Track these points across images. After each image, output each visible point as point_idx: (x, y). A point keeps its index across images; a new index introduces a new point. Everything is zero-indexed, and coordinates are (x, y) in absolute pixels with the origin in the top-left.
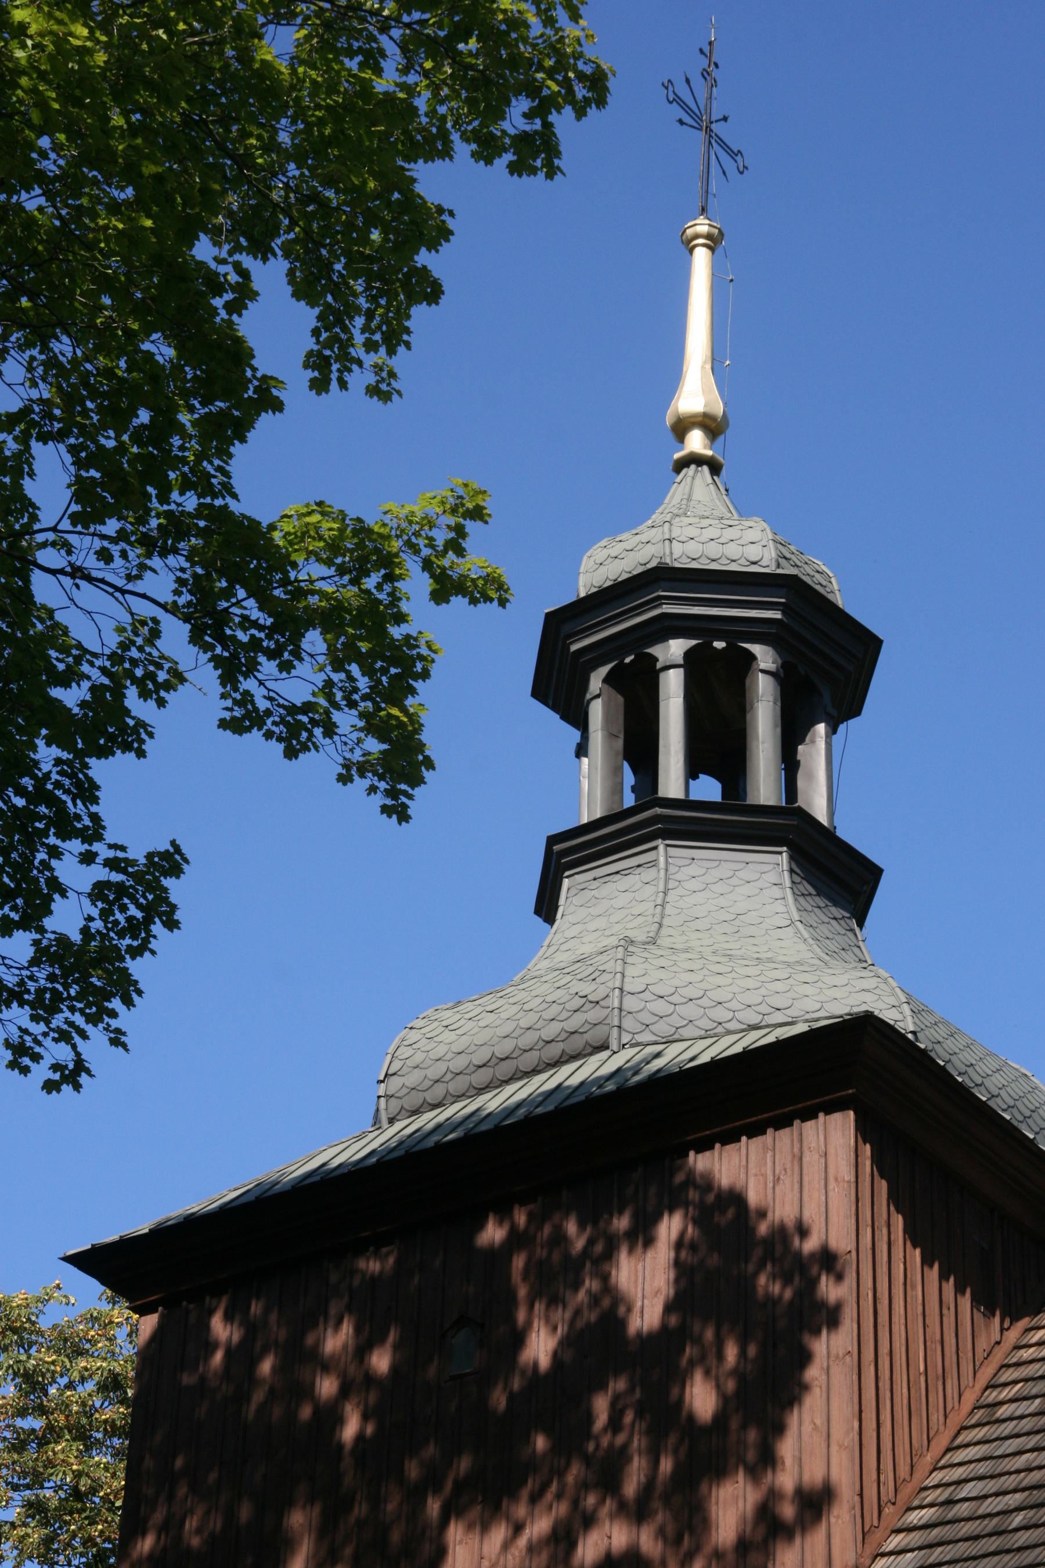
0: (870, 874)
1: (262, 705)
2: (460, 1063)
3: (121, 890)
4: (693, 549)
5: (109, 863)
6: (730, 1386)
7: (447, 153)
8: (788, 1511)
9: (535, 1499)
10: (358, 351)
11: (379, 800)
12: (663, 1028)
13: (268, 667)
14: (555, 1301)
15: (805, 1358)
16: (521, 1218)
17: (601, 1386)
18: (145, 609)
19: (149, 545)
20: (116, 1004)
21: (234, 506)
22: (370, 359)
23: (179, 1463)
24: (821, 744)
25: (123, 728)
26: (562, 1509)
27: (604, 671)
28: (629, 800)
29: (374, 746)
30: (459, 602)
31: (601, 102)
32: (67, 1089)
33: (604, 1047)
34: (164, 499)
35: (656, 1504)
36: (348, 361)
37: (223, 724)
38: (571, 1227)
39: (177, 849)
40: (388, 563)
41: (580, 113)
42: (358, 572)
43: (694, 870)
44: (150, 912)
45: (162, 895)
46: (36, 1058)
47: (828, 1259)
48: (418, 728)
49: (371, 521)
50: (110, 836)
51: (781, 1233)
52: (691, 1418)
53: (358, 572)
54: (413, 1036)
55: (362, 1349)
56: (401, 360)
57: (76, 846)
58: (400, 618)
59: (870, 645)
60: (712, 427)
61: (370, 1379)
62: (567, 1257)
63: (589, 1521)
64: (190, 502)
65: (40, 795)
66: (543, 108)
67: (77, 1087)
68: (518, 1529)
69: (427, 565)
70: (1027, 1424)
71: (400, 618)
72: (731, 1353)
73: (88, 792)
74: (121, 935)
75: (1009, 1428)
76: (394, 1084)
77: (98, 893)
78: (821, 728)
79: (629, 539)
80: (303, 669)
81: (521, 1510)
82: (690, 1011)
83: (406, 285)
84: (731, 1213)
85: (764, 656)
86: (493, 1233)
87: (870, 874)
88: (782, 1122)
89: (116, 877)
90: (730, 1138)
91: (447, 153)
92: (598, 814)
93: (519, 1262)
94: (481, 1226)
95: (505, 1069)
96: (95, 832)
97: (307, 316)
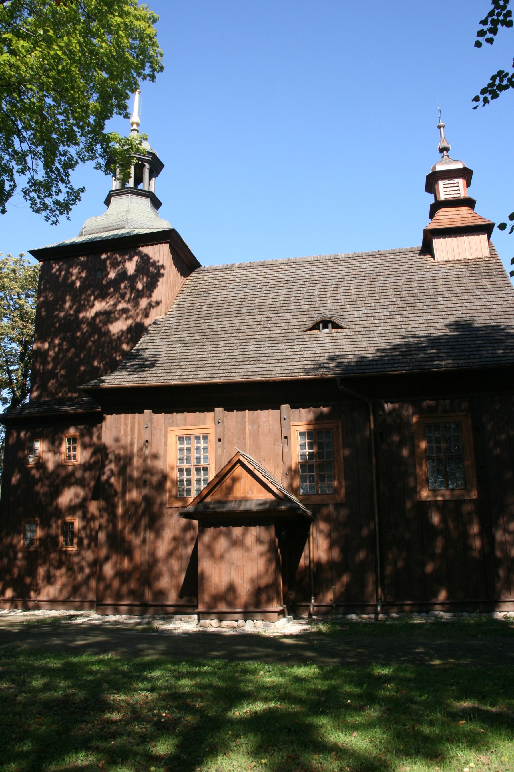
0: (160, 204)
2: (98, 227)
5: (69, 188)
6: (145, 284)
8: (154, 304)
9: (111, 297)
12: (134, 226)
14: (115, 268)
15: (158, 281)
16: (109, 254)
17: (123, 282)
23: (48, 286)
24: (154, 181)
26: (115, 300)
31: (162, 71)
32: (54, 225)
33: (124, 228)
35: (131, 301)
37: (94, 168)
39: (84, 188)
43: (135, 200)
44: (76, 197)
46: (49, 219)
47: (163, 266)
50: (71, 184)
52: (138, 289)
54: (89, 222)
55: (79, 273)
59: (163, 166)
60: (138, 125)
61: (81, 277)
62: (117, 262)
63: (120, 302)
67: (56, 225)
68: (107, 303)
70: (189, 294)
72: (145, 279)
73: (67, 175)
74: (71, 201)
75: (186, 294)
81: (108, 300)
82: (138, 224)
84: (146, 258)
85: (147, 166)
86: (103, 256)
87: (160, 204)
89: (70, 191)
90: (147, 245)
92: (118, 188)
93: (108, 262)
94: (102, 255)
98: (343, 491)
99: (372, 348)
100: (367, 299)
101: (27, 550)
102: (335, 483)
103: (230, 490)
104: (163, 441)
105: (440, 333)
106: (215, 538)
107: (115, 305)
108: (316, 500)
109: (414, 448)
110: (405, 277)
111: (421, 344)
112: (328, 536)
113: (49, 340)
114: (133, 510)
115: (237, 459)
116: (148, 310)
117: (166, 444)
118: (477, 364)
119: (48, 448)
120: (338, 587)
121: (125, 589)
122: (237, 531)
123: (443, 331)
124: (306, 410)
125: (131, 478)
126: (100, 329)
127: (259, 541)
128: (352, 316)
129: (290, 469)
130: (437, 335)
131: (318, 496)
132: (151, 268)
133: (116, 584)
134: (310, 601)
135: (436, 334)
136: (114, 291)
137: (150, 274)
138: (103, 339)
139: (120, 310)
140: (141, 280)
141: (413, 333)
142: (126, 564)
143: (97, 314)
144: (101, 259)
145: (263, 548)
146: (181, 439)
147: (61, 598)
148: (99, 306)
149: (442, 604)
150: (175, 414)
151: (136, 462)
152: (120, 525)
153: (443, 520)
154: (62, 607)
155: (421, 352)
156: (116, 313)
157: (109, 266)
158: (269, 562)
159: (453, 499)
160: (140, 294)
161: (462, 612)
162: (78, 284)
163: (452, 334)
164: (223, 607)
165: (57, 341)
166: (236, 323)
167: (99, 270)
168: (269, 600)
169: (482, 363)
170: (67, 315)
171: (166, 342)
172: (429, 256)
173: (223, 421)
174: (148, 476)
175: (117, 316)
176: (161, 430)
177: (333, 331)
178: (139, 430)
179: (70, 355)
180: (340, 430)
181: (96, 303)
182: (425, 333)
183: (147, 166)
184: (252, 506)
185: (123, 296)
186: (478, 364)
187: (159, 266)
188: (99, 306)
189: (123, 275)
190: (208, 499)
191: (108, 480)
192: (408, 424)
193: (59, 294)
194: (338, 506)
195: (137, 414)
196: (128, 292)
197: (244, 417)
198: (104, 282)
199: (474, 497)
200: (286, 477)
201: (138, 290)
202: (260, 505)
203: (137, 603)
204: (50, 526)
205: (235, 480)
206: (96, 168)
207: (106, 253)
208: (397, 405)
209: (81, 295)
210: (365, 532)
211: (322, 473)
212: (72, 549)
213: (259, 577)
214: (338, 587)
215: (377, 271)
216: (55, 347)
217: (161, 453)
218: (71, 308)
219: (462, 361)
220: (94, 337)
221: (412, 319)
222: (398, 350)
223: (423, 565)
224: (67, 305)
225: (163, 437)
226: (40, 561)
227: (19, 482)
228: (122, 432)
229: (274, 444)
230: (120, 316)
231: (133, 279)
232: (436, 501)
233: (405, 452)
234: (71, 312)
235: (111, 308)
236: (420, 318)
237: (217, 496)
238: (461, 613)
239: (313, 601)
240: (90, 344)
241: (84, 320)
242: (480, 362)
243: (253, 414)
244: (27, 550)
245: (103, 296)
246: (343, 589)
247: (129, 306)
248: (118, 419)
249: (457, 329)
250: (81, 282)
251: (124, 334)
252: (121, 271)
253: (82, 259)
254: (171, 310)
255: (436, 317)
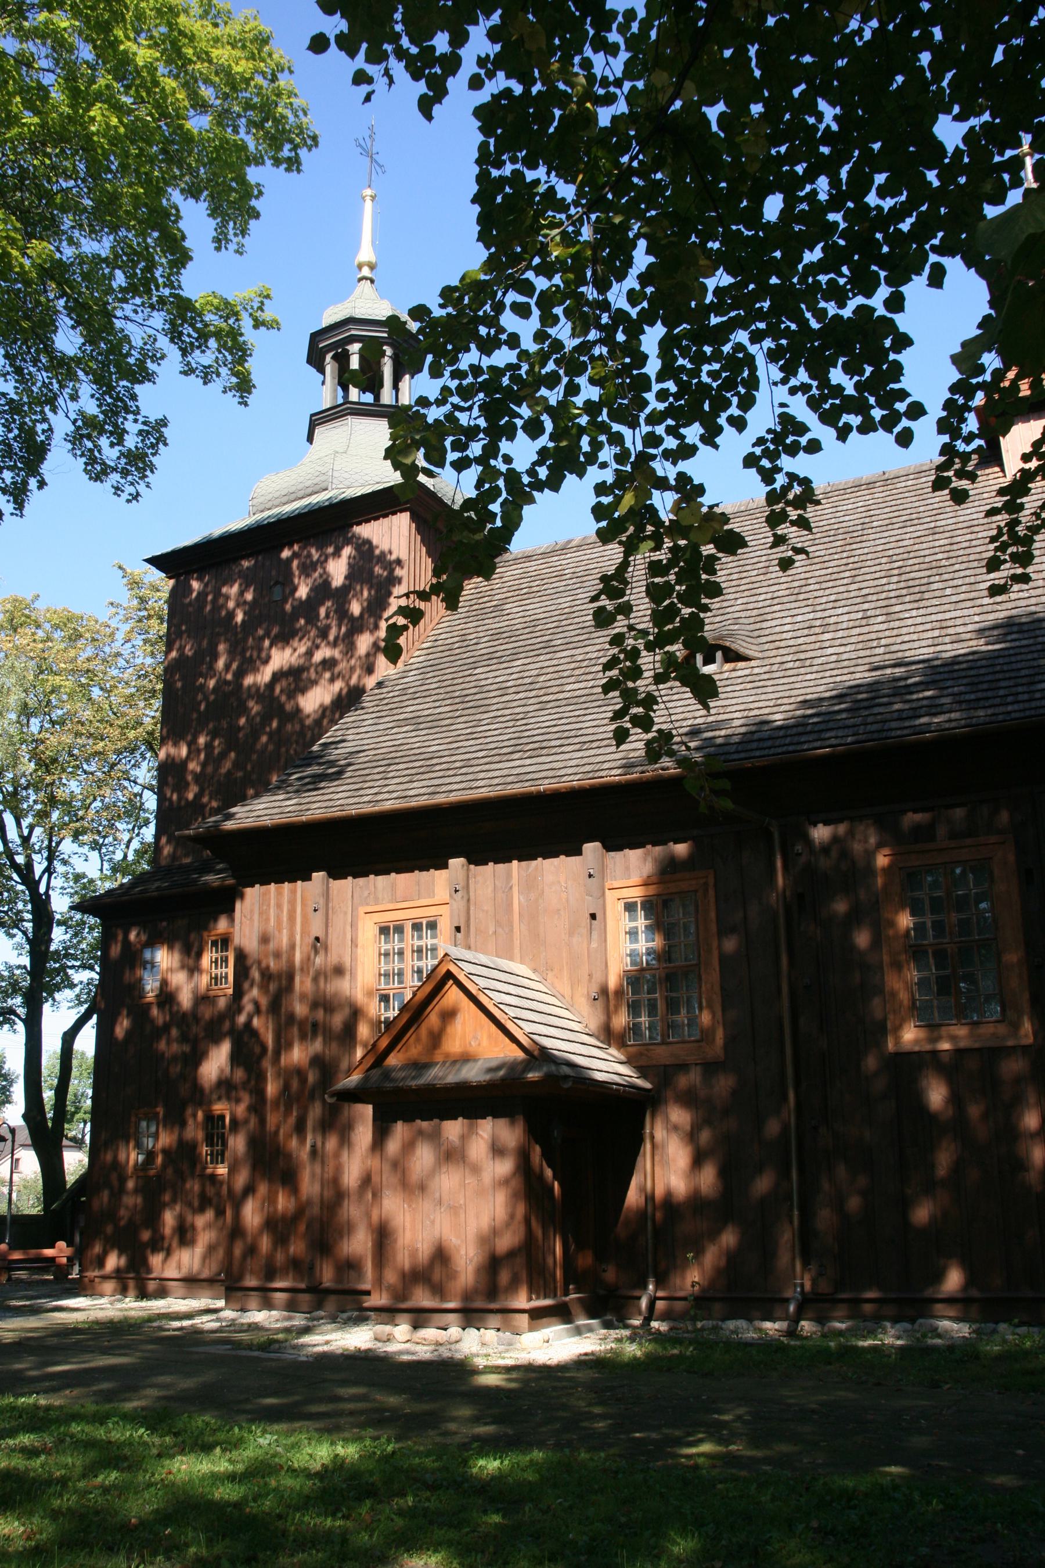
1: (194, 366)
2: (277, 495)
3: (148, 433)
4: (363, 311)
7: (263, 163)
9: (300, 640)
10: (231, 236)
11: (237, 399)
12: (347, 483)
13: (197, 352)
14: (308, 576)
17: (323, 604)
18: (151, 332)
19: (152, 307)
20: (148, 473)
21: (181, 293)
22: (235, 240)
25: (148, 374)
26: (309, 644)
27: (331, 354)
28: (340, 401)
29: (234, 380)
30: (263, 329)
31: (316, 145)
34: (157, 290)
36: (228, 241)
38: (313, 551)
40: (236, 314)
41: (310, 150)
42: (226, 319)
44: (158, 440)
45: (162, 435)
47: (399, 562)
48: (249, 374)
49: (230, 300)
50: (143, 413)
51: (383, 553)
53: (226, 319)
55: (241, 593)
56: (246, 241)
57: (131, 417)
58: (241, 335)
60: (372, 267)
61: (245, 602)
63: (318, 647)
64: (167, 292)
65: (118, 399)
66: (295, 148)
68: (295, 650)
69: (251, 315)
71: (241, 335)
72: (366, 594)
73: (134, 397)
76: (255, 501)
77: (140, 433)
78: (407, 377)
79: (340, 307)
80: (208, 353)
83: (248, 212)
85: (388, 351)
86: (286, 554)
88: (385, 516)
90: (368, 521)
91: (263, 163)
93: (295, 563)
94: (282, 550)
95: (292, 497)
96: (137, 412)
97: (212, 223)
98: (720, 1034)
99: (792, 700)
100: (824, 586)
101: (141, 1174)
102: (706, 1018)
103: (436, 1039)
104: (349, 937)
105: (961, 649)
106: (409, 1147)
107: (309, 653)
108: (662, 1055)
109: (880, 927)
110: (926, 526)
111: (906, 679)
112: (691, 1137)
113: (189, 738)
114: (295, 1084)
115: (444, 971)
116: (371, 659)
117: (354, 943)
118: (1013, 715)
119: (182, 961)
120: (711, 1256)
121: (280, 1257)
122: (453, 1129)
123: (971, 643)
124: (639, 852)
125: (291, 1017)
126: (282, 706)
127: (497, 1150)
128: (778, 629)
129: (604, 991)
130: (953, 653)
131: (664, 1047)
132: (377, 569)
133: (265, 1243)
134: (645, 1287)
135: (950, 650)
136: (307, 623)
137: (375, 581)
138: (289, 727)
139: (317, 665)
140: (358, 595)
141: (900, 655)
142: (283, 1203)
143: (277, 676)
144: (280, 559)
145: (505, 1167)
146: (384, 930)
147: (206, 1274)
148: (281, 658)
149: (950, 1301)
150: (372, 876)
151: (302, 984)
152: (272, 1119)
153: (955, 1099)
154: (208, 1293)
155: (897, 699)
156: (312, 670)
157: (297, 573)
158: (515, 1196)
159: (977, 1045)
160: (356, 626)
161: (997, 1323)
162: (239, 617)
163: (990, 647)
164: (423, 1299)
165: (202, 740)
166: (533, 670)
167: (277, 583)
168: (513, 1287)
169: (1028, 713)
170: (222, 683)
171: (386, 723)
172: (997, 469)
173: (467, 887)
174: (320, 1014)
175: (313, 676)
176: (346, 913)
177: (728, 666)
178: (304, 916)
179: (227, 765)
180: (711, 893)
181: (274, 652)
182: (926, 653)
183: (388, 351)
184: (472, 1073)
185: (324, 634)
186: (1017, 715)
187: (390, 563)
188: (281, 658)
189: (323, 590)
190: (393, 1060)
191: (248, 1024)
192: (870, 869)
193: (205, 643)
194: (710, 1068)
195: (299, 883)
196: (334, 623)
197: (509, 876)
198: (288, 607)
199: (1030, 1040)
200: (593, 1006)
201: (352, 619)
202: (490, 1070)
203: (303, 1286)
204: (183, 1124)
205: (449, 1015)
206: (185, 373)
207: (290, 545)
208: (842, 829)
209: (245, 640)
210: (773, 1128)
211: (674, 995)
212: (222, 1170)
213: (495, 1232)
214: (711, 1256)
215: (867, 520)
216: (199, 751)
217: (347, 963)
218: (227, 667)
219: (981, 713)
220: (270, 725)
221: (910, 622)
222: (848, 699)
223: (905, 1205)
224: (221, 663)
225: (349, 928)
226: (167, 1197)
227: (129, 1033)
228: (272, 922)
229: (571, 933)
230: (319, 675)
231: (342, 596)
232: (935, 1053)
233: (862, 939)
234: (229, 677)
235: (302, 661)
236: (929, 619)
237: (412, 1049)
238: (991, 1326)
239: (651, 1287)
240: (264, 739)
241: (255, 692)
242: (1025, 710)
243: (528, 867)
244: (141, 1174)
245: (284, 639)
246: (723, 1263)
247: (337, 653)
248: (264, 894)
249: (1006, 634)
250: (245, 614)
251: (328, 713)
252: (320, 581)
253: (246, 564)
254: (418, 653)
255: (966, 612)
